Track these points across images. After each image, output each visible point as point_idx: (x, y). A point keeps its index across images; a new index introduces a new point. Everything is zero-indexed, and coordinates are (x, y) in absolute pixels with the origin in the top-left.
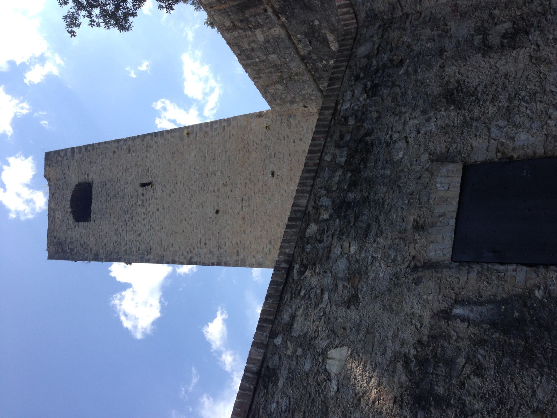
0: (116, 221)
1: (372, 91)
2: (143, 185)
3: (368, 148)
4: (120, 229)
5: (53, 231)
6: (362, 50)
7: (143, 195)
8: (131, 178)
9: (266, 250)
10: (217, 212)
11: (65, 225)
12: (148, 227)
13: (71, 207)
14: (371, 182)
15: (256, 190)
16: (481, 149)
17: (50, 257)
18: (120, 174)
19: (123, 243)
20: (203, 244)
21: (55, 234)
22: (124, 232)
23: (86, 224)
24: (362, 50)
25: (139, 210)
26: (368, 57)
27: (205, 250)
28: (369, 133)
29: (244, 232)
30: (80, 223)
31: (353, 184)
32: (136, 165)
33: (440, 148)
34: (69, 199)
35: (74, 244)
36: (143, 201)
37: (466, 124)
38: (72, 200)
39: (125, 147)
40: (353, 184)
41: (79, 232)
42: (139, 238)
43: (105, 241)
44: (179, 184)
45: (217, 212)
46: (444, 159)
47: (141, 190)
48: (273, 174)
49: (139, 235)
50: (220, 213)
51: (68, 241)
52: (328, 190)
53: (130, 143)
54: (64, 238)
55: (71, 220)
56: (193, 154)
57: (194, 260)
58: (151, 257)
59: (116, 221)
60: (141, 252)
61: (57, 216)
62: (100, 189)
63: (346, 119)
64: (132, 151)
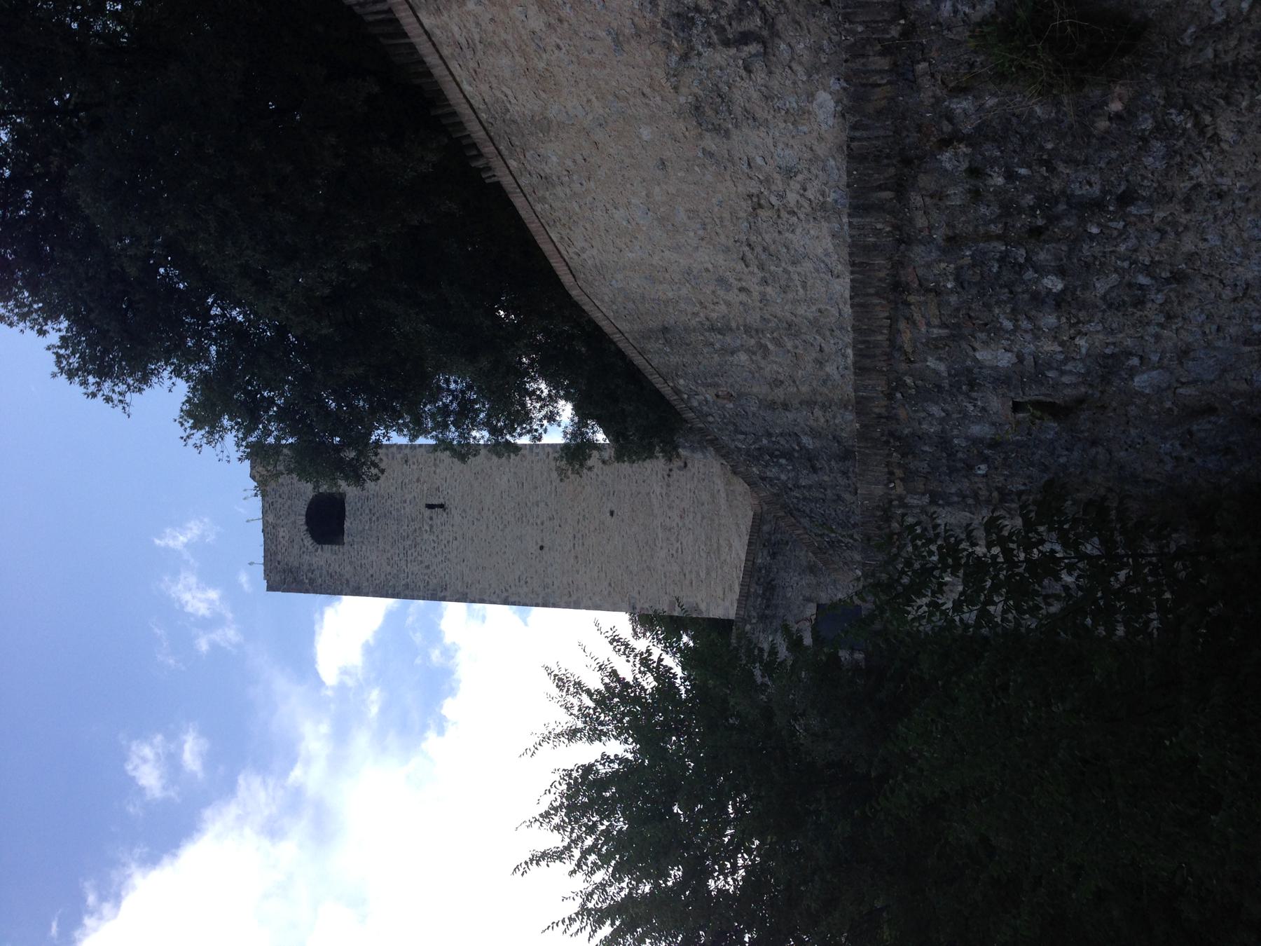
0: (388, 548)
1: (773, 555)
2: (430, 507)
3: (773, 588)
4: (396, 558)
5: (276, 554)
6: (766, 528)
7: (431, 519)
8: (411, 496)
9: (606, 593)
10: (542, 548)
11: (296, 547)
12: (440, 558)
13: (307, 523)
14: (776, 606)
15: (592, 529)
16: (824, 598)
17: (271, 588)
18: (393, 489)
19: (402, 576)
20: (522, 582)
21: (279, 557)
22: (403, 562)
23: (336, 548)
24: (766, 528)
25: (426, 536)
26: (769, 533)
27: (525, 589)
28: (773, 580)
29: (578, 572)
30: (326, 547)
31: (768, 607)
32: (418, 480)
33: (807, 595)
34: (304, 512)
35: (317, 573)
36: (431, 527)
37: (818, 584)
38: (307, 515)
39: (399, 456)
40: (768, 607)
41: (324, 557)
42: (428, 571)
43: (371, 572)
44: (486, 510)
45: (542, 548)
46: (809, 600)
47: (427, 512)
48: (612, 513)
49: (428, 567)
50: (546, 549)
51: (305, 568)
52: (754, 607)
53: (407, 451)
54: (296, 564)
55: (308, 541)
56: (505, 478)
57: (513, 600)
58: (448, 594)
59: (388, 548)
60: (430, 587)
61: (281, 534)
62: (359, 505)
63: (760, 569)
64: (410, 462)
